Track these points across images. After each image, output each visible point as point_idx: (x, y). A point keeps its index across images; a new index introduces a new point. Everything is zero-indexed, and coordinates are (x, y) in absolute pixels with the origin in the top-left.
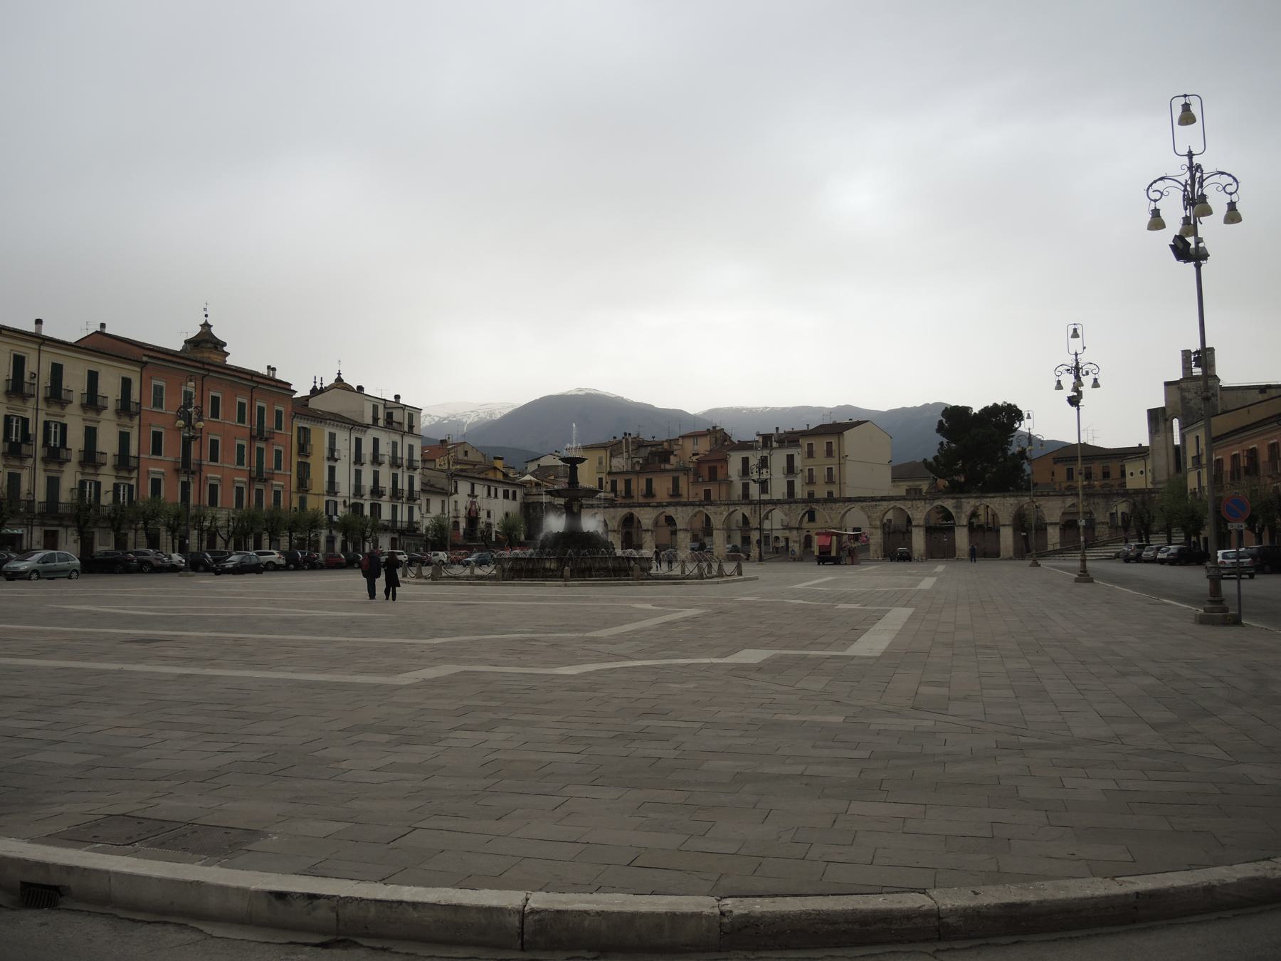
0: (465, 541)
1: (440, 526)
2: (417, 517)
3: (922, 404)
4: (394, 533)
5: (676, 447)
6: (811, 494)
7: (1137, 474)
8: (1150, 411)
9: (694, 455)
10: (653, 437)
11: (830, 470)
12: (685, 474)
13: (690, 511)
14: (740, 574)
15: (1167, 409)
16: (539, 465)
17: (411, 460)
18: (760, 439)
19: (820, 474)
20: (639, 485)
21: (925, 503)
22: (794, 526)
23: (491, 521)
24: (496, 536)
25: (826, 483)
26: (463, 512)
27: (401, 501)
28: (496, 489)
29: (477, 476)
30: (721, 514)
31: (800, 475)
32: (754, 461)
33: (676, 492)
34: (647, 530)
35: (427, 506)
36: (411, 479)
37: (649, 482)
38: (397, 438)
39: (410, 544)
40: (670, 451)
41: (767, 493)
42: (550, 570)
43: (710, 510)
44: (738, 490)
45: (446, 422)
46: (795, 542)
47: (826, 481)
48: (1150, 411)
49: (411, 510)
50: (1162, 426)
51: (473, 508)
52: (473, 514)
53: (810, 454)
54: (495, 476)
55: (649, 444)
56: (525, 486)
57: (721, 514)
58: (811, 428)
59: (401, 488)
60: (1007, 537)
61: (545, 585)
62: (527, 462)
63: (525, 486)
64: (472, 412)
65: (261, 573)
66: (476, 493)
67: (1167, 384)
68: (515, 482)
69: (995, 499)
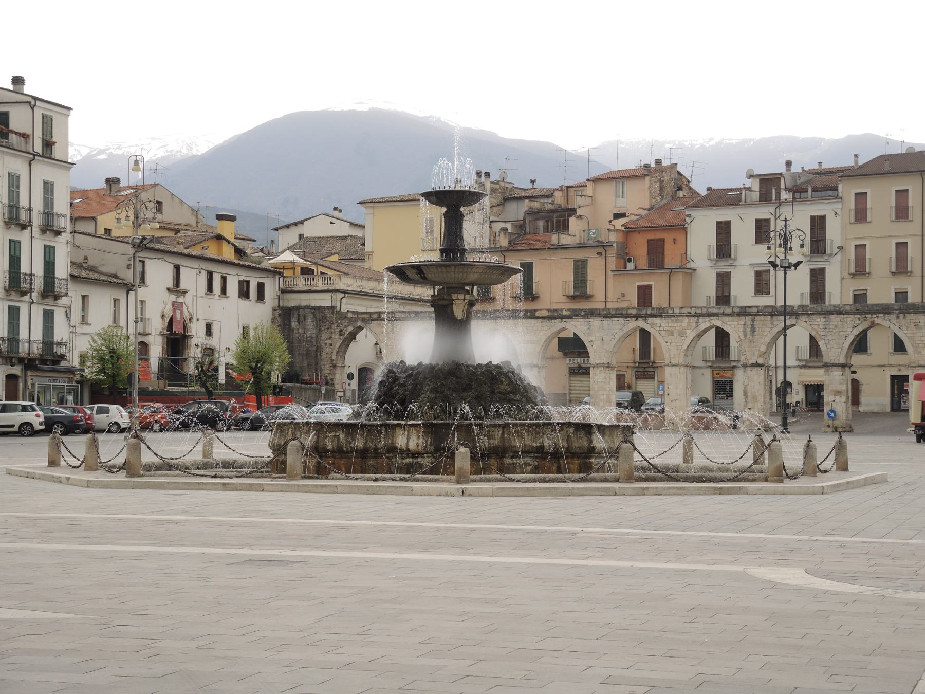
0: (162, 383)
1: (112, 352)
2: (60, 332)
4: (12, 365)
5: (579, 201)
6: (860, 297)
9: (617, 216)
10: (533, 182)
11: (901, 247)
12: (599, 254)
13: (617, 327)
14: (843, 467)
16: (301, 236)
17: (48, 214)
18: (755, 185)
22: (836, 362)
23: (214, 342)
24: (227, 374)
25: (893, 273)
26: (156, 326)
27: (27, 298)
28: (224, 279)
29: (186, 251)
30: (682, 334)
31: (838, 258)
33: (580, 291)
35: (83, 309)
36: (49, 252)
38: (18, 165)
39: (45, 389)
40: (568, 210)
41: (768, 293)
42: (407, 452)
43: (657, 327)
44: (707, 288)
45: (103, 157)
46: (838, 393)
47: (894, 270)
49: (48, 317)
51: (178, 317)
52: (178, 329)
53: (861, 215)
54: (220, 251)
55: (524, 194)
56: (281, 274)
57: (682, 334)
58: (861, 162)
59: (28, 272)
61: (411, 492)
62: (276, 229)
63: (281, 274)
64: (153, 139)
66: (183, 286)
68: (262, 266)
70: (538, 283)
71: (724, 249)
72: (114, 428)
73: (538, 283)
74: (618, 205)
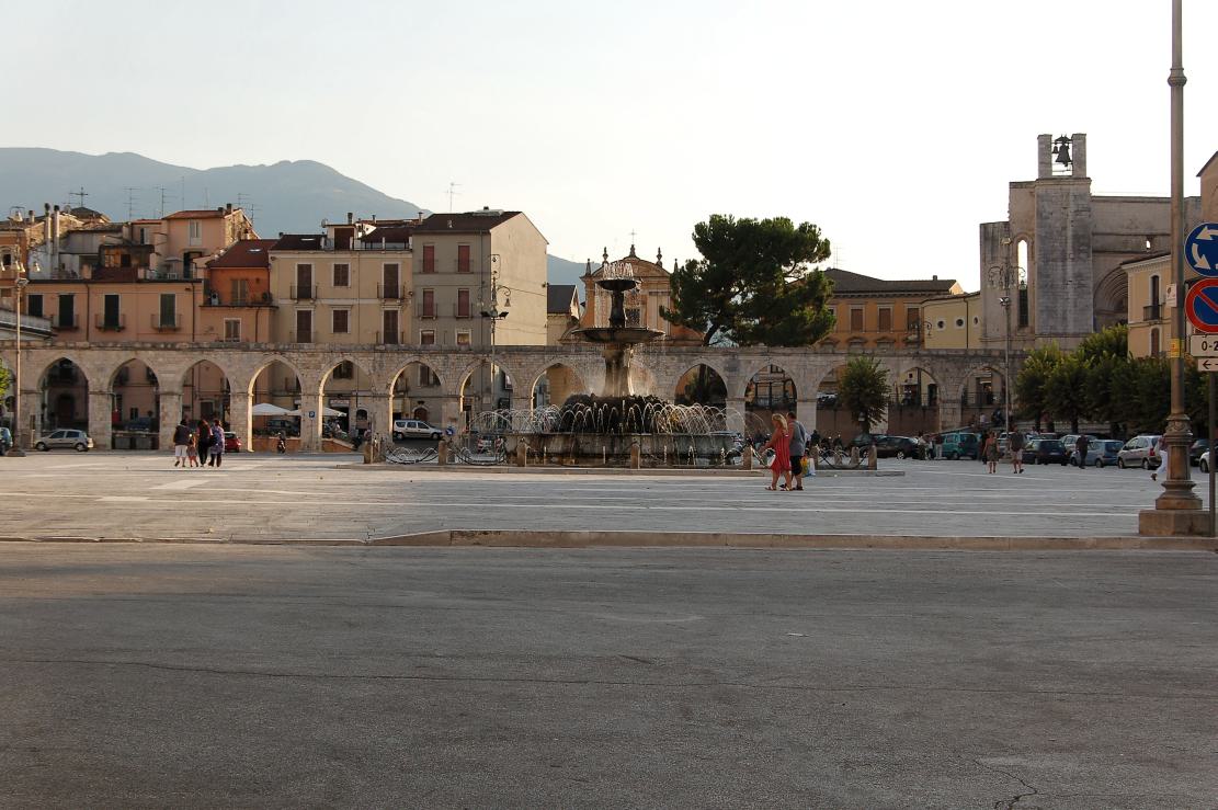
3: (104, 152)
7: (950, 324)
8: (984, 227)
15: (1013, 226)
18: (331, 235)
19: (446, 300)
21: (680, 361)
32: (322, 277)
34: (171, 394)
48: (984, 227)
53: (428, 265)
60: (100, 413)
65: (1065, 465)
67: (1014, 186)
69: (791, 358)
70: (78, 316)
71: (304, 291)
72: (41, 447)
73: (78, 316)
74: (193, 244)
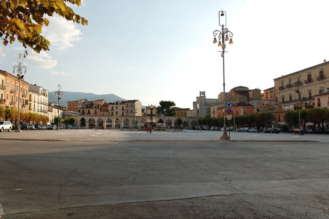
19: (129, 111)
20: (86, 111)
37: (89, 111)
50: (195, 105)
67: (275, 80)
